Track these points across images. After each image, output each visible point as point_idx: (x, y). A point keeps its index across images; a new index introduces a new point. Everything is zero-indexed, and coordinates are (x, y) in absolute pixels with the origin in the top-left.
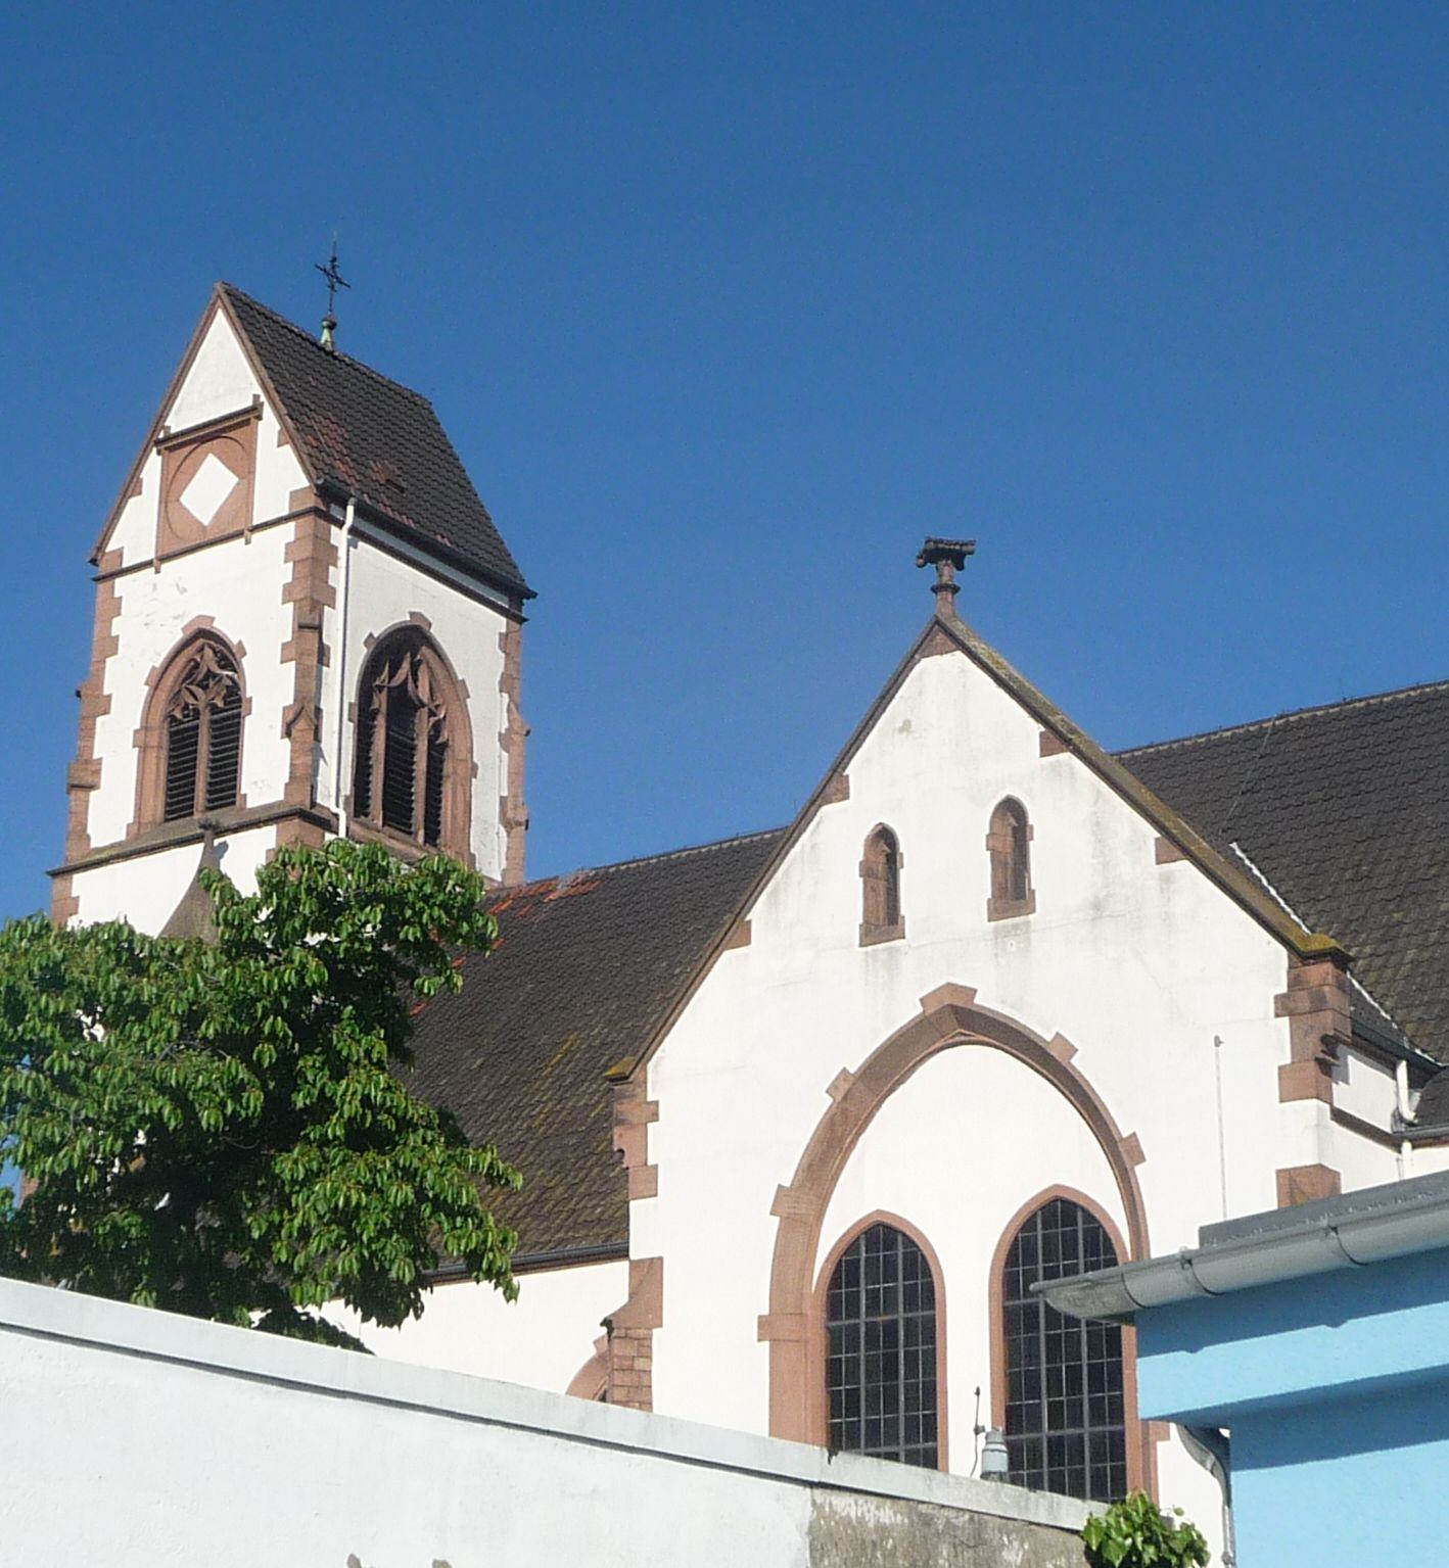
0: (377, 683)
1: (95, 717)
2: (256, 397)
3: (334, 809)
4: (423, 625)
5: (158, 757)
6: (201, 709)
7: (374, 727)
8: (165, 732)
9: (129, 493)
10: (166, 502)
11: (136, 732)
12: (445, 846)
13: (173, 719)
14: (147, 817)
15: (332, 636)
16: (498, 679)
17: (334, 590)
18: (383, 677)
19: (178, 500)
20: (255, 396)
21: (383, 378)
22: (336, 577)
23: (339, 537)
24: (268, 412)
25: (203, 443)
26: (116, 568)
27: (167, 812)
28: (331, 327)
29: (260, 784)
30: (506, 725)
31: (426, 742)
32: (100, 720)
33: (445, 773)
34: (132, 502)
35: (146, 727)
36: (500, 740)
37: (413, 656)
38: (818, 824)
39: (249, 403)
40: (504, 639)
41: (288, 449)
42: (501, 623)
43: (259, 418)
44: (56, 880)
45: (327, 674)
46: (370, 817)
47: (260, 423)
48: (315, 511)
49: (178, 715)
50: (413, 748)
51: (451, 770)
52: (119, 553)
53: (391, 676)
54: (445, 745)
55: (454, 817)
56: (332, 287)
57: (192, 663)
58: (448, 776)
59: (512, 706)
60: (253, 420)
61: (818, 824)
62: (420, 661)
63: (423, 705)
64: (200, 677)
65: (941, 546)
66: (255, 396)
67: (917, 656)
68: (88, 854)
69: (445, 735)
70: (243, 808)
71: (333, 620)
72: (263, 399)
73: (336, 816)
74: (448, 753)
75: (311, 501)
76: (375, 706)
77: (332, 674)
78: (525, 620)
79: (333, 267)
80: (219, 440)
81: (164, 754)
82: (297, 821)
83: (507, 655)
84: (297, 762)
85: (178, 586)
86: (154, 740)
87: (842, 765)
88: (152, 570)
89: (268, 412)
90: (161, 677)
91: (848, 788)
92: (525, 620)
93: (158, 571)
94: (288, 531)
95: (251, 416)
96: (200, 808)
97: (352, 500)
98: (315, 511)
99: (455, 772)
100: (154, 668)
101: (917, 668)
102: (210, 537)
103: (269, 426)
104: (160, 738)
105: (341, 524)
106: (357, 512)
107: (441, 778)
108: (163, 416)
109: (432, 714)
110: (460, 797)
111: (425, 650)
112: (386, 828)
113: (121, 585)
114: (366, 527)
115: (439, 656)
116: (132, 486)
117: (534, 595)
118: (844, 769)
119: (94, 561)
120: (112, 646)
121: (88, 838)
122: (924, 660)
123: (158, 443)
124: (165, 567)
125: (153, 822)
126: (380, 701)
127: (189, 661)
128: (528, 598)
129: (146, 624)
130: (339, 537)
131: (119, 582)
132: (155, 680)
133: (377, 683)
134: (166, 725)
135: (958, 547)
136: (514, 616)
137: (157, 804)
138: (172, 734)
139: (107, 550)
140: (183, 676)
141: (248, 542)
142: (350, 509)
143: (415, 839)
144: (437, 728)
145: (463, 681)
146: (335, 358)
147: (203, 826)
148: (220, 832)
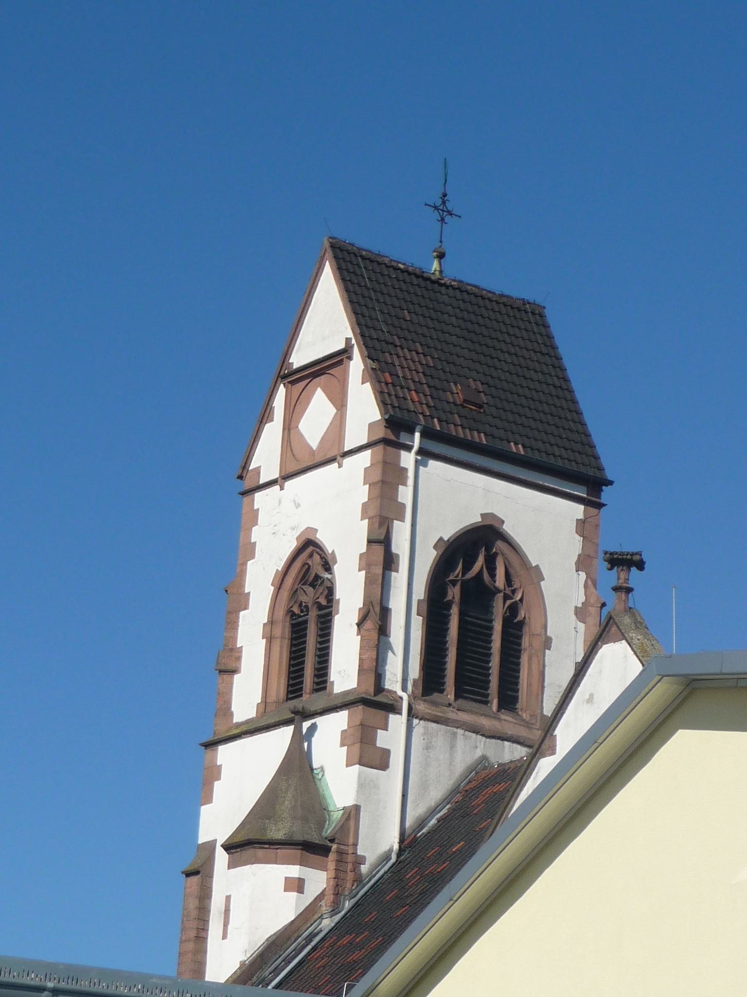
0: (451, 578)
1: (239, 611)
2: (348, 340)
3: (400, 693)
4: (496, 524)
5: (281, 647)
6: (310, 606)
7: (450, 615)
8: (288, 624)
9: (264, 421)
10: (289, 430)
11: (264, 625)
12: (522, 709)
13: (293, 614)
14: (272, 697)
15: (400, 545)
16: (575, 559)
17: (403, 506)
18: (457, 572)
19: (297, 427)
20: (347, 339)
21: (494, 293)
22: (405, 494)
23: (408, 459)
24: (356, 353)
25: (315, 377)
26: (253, 485)
27: (288, 692)
28: (441, 256)
29: (342, 674)
30: (582, 598)
31: (501, 623)
32: (242, 613)
33: (523, 647)
34: (268, 427)
35: (271, 622)
36: (576, 614)
37: (488, 550)
38: (537, 773)
39: (341, 346)
40: (582, 526)
41: (368, 385)
42: (578, 510)
43: (350, 358)
44: (207, 751)
45: (395, 578)
46: (445, 693)
47: (351, 362)
48: (385, 441)
49: (296, 610)
50: (491, 628)
51: (527, 644)
52: (258, 470)
53: (464, 573)
54: (521, 624)
55: (529, 685)
56: (442, 220)
57: (307, 566)
58: (525, 649)
59: (590, 583)
60: (345, 359)
61: (537, 773)
62: (496, 554)
63: (499, 591)
64: (311, 579)
65: (615, 556)
66: (347, 339)
67: (600, 643)
68: (230, 729)
69: (522, 614)
70: (331, 693)
71: (401, 533)
72: (353, 341)
73: (401, 698)
74: (526, 629)
75: (381, 433)
76: (449, 597)
77: (399, 579)
78: (604, 505)
79: (444, 203)
80: (323, 376)
81: (287, 643)
82: (361, 707)
83: (585, 538)
84: (364, 657)
85: (294, 501)
86: (278, 632)
87: (552, 728)
88: (277, 487)
89: (356, 353)
90: (283, 580)
91: (555, 746)
92: (604, 505)
93: (282, 488)
94: (365, 457)
95: (344, 357)
96: (308, 691)
97: (418, 428)
98: (385, 441)
99: (531, 645)
100: (277, 570)
101: (600, 652)
102: (318, 459)
103: (357, 365)
104: (283, 630)
105: (409, 448)
106: (423, 436)
107: (520, 651)
108: (287, 354)
109: (506, 597)
110: (535, 667)
111: (499, 544)
112: (460, 701)
113: (259, 497)
114: (435, 447)
115: (512, 546)
116: (265, 415)
117: (611, 483)
118: (554, 730)
119: (241, 477)
120: (250, 551)
121: (232, 714)
122: (605, 646)
123: (285, 377)
124: (288, 484)
125: (277, 702)
126: (454, 593)
127: (303, 566)
128: (606, 486)
129: (274, 533)
130: (408, 459)
131: (258, 496)
132: (277, 583)
133: (451, 578)
134: (288, 618)
135: (629, 557)
136: (593, 503)
137: (280, 687)
138: (293, 626)
139: (250, 468)
140: (300, 577)
141: (340, 466)
142: (417, 435)
143: (491, 708)
144: (513, 609)
145: (537, 567)
146: (441, 285)
147: (293, 712)
148: (306, 715)
